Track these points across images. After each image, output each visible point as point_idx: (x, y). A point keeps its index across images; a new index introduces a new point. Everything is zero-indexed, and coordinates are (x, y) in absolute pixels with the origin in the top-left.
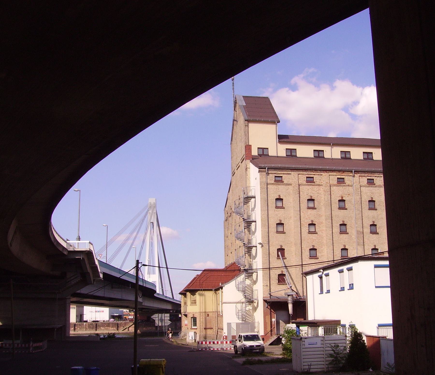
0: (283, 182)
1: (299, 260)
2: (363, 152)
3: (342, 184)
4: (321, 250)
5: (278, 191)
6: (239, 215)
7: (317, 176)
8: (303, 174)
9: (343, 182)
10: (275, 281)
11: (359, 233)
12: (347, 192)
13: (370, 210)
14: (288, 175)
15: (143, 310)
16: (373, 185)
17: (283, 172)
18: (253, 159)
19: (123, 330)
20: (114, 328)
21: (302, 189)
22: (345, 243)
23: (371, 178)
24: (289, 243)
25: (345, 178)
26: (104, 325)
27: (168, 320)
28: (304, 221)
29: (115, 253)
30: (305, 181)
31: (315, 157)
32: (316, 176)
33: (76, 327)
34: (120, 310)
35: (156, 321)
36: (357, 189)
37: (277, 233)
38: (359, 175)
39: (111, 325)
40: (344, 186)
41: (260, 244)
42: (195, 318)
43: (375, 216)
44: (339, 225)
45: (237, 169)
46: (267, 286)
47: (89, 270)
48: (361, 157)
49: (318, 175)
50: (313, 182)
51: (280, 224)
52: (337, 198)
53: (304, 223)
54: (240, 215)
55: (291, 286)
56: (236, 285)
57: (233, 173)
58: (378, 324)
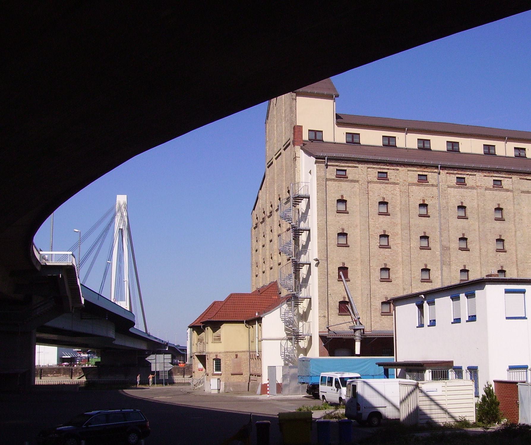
0: (347, 178)
1: (366, 283)
3: (424, 183)
4: (396, 270)
5: (341, 189)
6: (287, 220)
7: (392, 171)
8: (374, 168)
9: (425, 180)
10: (335, 310)
11: (445, 249)
12: (431, 194)
13: (460, 219)
14: (353, 168)
16: (465, 186)
17: (501, 175)
18: (304, 147)
19: (79, 378)
21: (372, 188)
22: (426, 261)
23: (462, 176)
24: (353, 260)
25: (428, 176)
26: (52, 371)
27: (169, 364)
28: (373, 231)
30: (376, 177)
31: (448, 151)
32: (390, 170)
34: (74, 351)
35: (152, 364)
36: (444, 190)
37: (338, 246)
38: (446, 172)
39: (62, 371)
40: (427, 186)
41: (316, 260)
42: (219, 360)
43: (466, 226)
44: (419, 238)
45: (276, 159)
46: (324, 316)
47: (68, 293)
48: (444, 148)
49: (394, 169)
50: (386, 179)
51: (343, 234)
52: (417, 201)
53: (374, 234)
54: (288, 221)
55: (358, 317)
56: (280, 315)
57: (269, 164)
58: (509, 366)
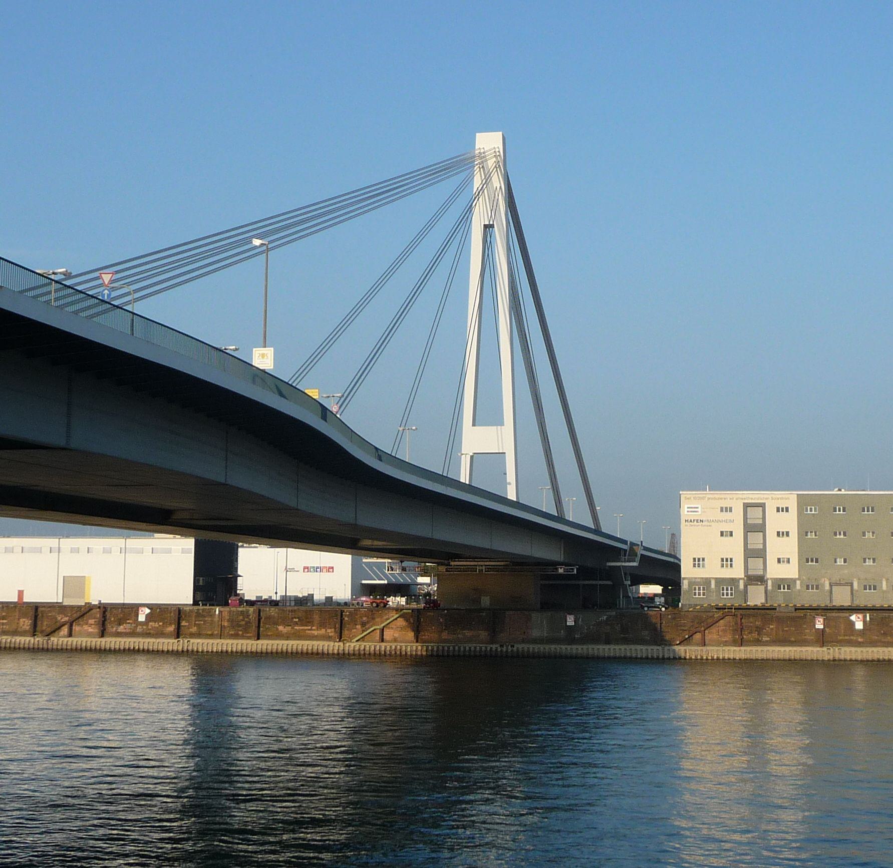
2: (23, 591)
15: (452, 563)
20: (329, 631)
29: (413, 247)
33: (183, 623)
